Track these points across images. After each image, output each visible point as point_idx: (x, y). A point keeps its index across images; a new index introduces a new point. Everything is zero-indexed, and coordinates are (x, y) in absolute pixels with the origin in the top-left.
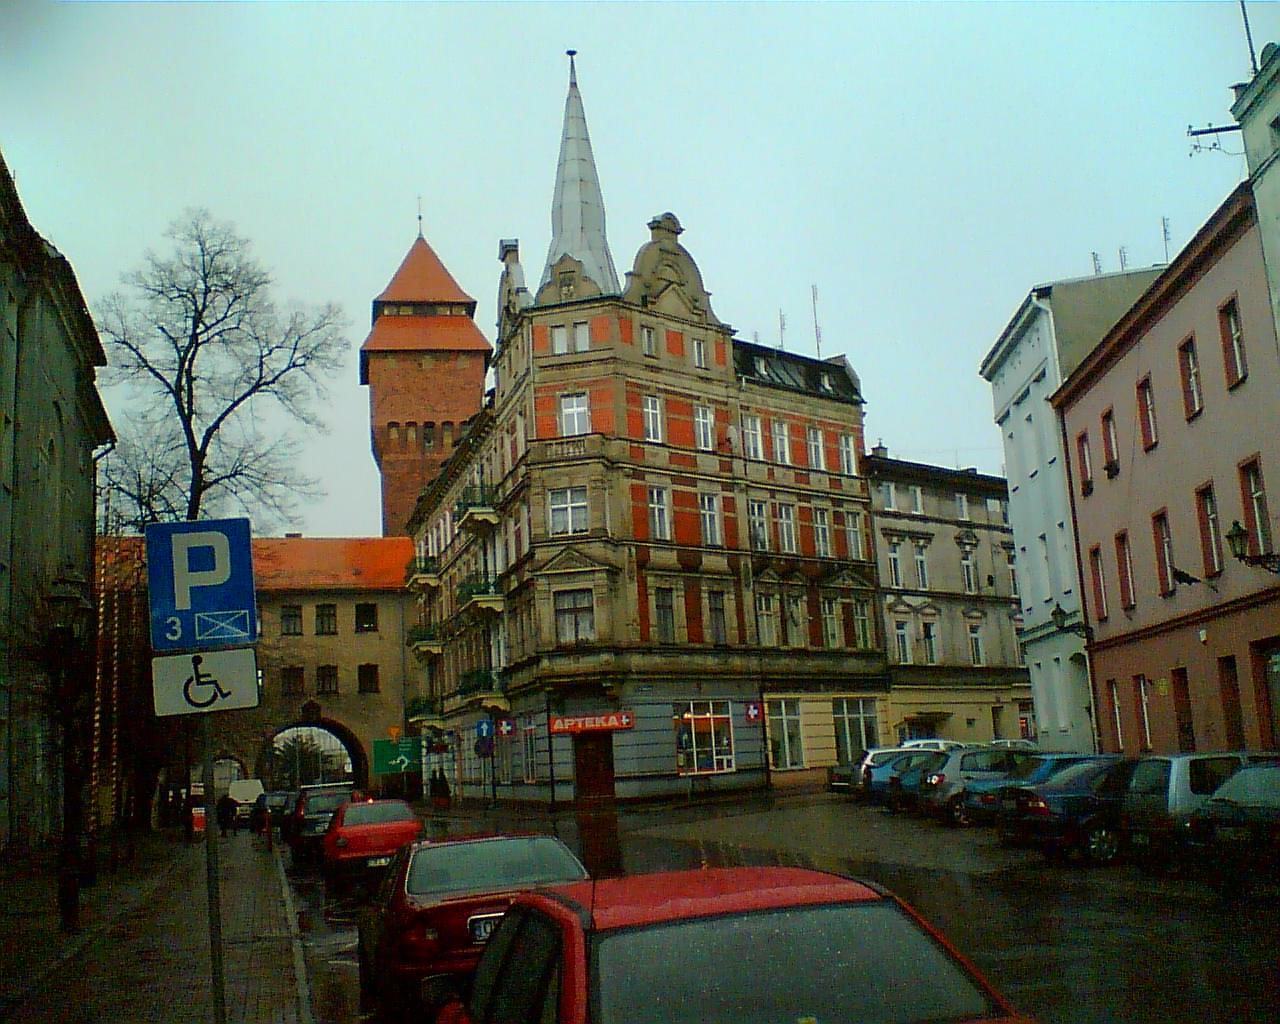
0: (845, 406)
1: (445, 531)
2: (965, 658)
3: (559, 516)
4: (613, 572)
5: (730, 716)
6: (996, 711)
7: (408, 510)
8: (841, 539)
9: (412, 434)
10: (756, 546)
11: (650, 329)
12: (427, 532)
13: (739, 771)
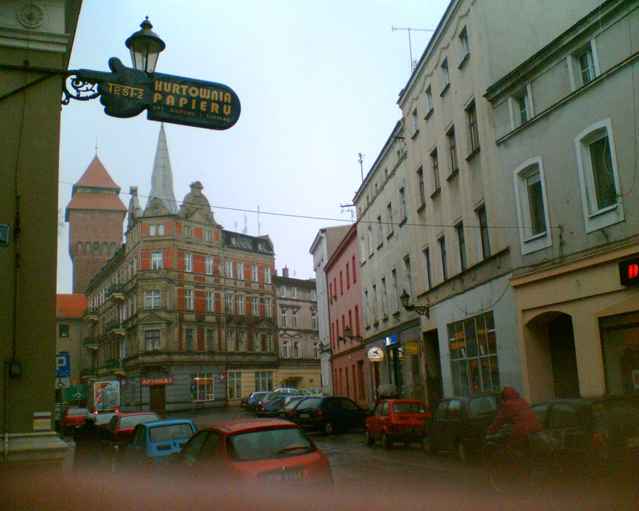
3: (149, 301)
4: (169, 323)
8: (262, 308)
9: (88, 247)
11: (189, 227)
13: (215, 400)
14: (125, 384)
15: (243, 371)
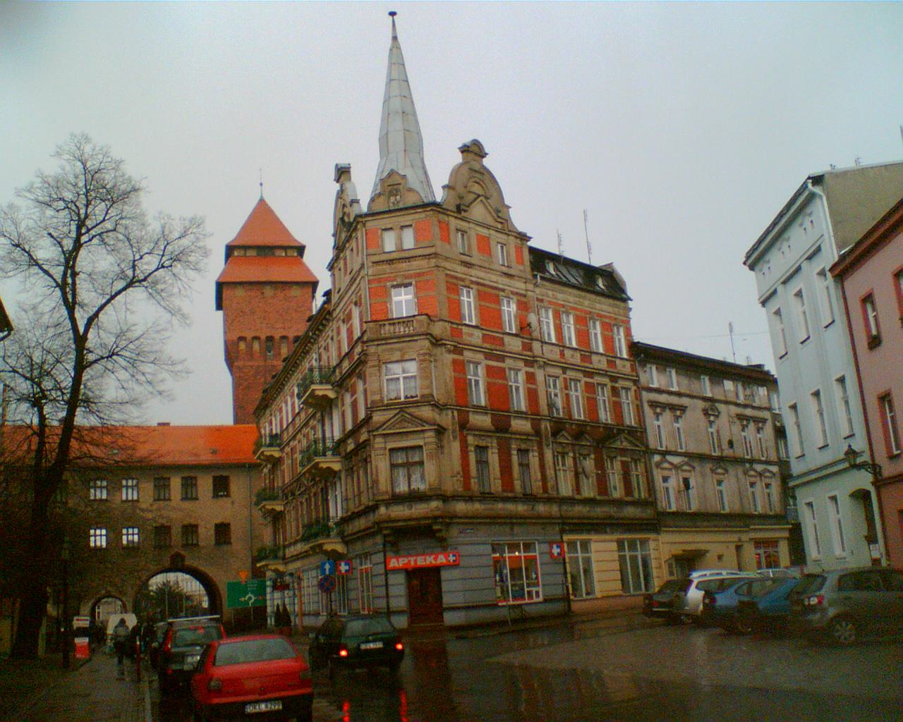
0: (616, 302)
2: (713, 506)
3: (392, 386)
4: (440, 431)
5: (537, 554)
6: (738, 548)
7: (255, 399)
8: (617, 408)
9: (256, 346)
10: (553, 412)
11: (464, 232)
12: (271, 415)
13: (545, 601)
14: (346, 571)
15: (593, 537)
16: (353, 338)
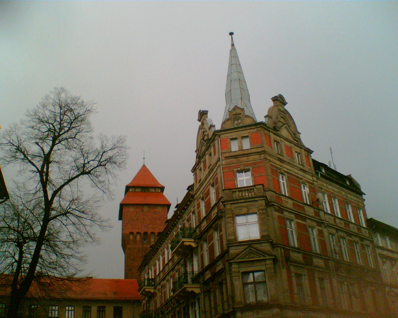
1: (152, 274)
4: (275, 260)
9: (138, 237)
11: (278, 143)
16: (201, 218)
